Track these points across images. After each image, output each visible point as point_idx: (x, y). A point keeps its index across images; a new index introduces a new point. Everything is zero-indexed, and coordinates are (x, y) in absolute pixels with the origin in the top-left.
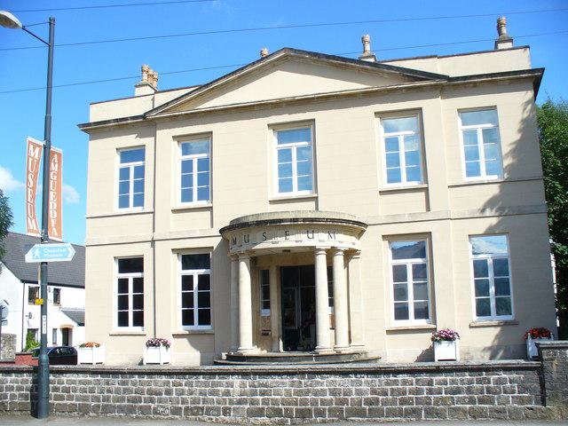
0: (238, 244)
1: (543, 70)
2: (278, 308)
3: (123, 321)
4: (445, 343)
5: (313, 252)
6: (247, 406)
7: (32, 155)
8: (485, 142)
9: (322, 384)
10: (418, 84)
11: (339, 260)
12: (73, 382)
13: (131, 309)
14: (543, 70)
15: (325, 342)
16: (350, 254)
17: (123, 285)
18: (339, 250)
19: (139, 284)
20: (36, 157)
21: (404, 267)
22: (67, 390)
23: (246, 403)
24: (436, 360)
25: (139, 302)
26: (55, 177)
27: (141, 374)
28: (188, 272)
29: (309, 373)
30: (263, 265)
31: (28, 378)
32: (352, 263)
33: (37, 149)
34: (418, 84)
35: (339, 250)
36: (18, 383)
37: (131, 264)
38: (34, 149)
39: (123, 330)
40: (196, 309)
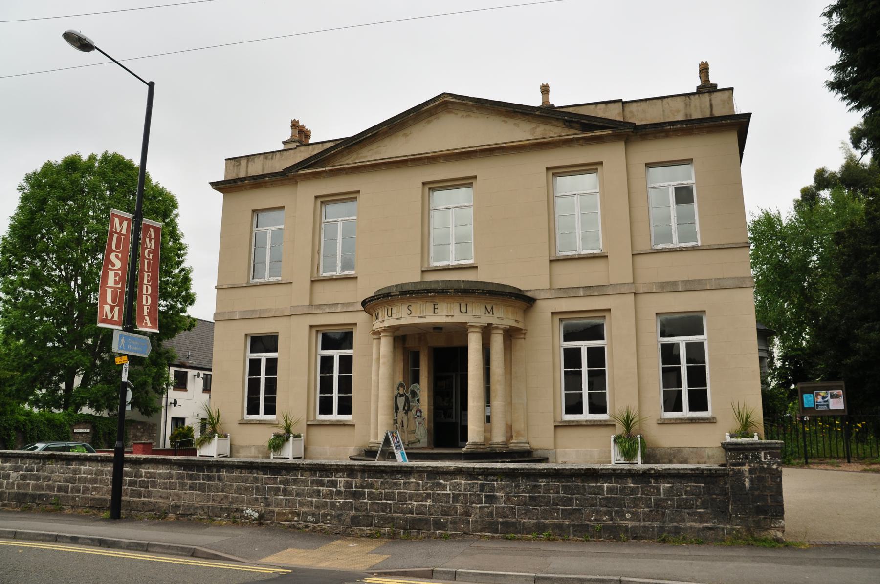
0: (380, 319)
1: (749, 115)
2: (429, 396)
3: (253, 408)
4: (291, 429)
5: (462, 330)
6: (353, 513)
7: (118, 231)
8: (677, 203)
9: (444, 487)
10: (598, 133)
11: (497, 342)
12: (152, 475)
13: (261, 393)
14: (749, 115)
15: (474, 433)
16: (511, 335)
17: (255, 365)
18: (497, 328)
19: (272, 365)
20: (124, 232)
21: (578, 350)
22: (144, 484)
23: (351, 508)
24: (613, 463)
25: (271, 386)
26: (151, 255)
27: (231, 467)
28: (255, 356)
29: (428, 472)
30: (412, 344)
31: (109, 468)
32: (520, 344)
33: (125, 223)
34: (598, 133)
35: (497, 328)
36: (91, 474)
37: (264, 342)
38: (121, 223)
39: (655, 327)
40: (335, 395)
